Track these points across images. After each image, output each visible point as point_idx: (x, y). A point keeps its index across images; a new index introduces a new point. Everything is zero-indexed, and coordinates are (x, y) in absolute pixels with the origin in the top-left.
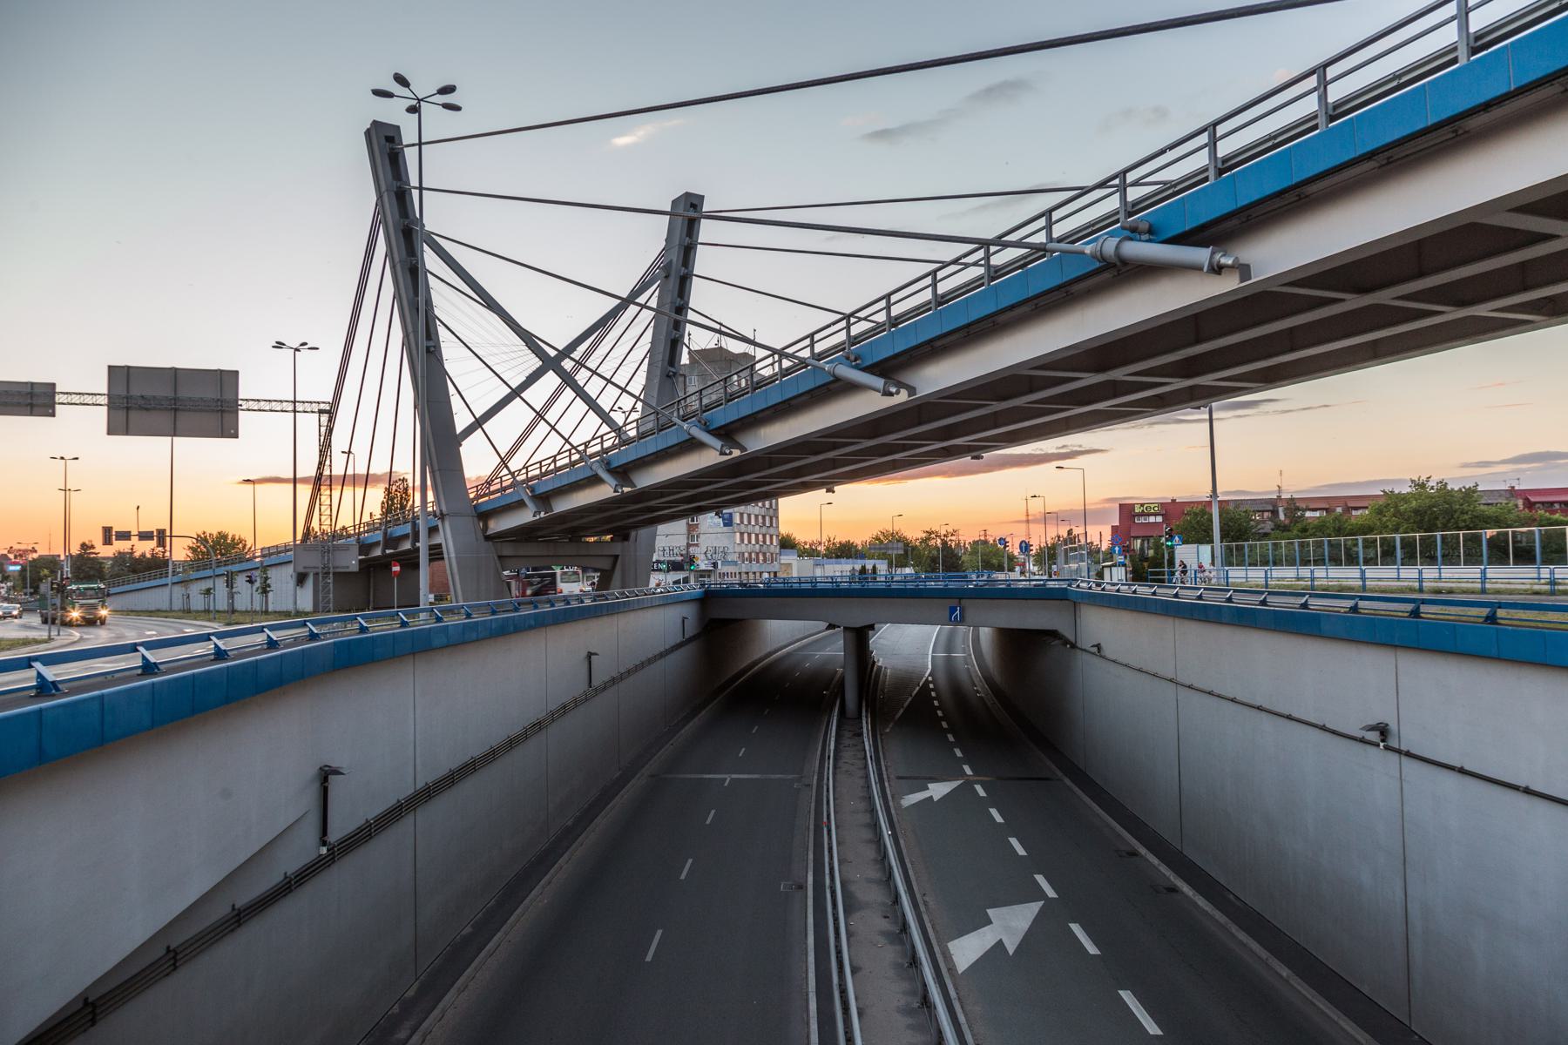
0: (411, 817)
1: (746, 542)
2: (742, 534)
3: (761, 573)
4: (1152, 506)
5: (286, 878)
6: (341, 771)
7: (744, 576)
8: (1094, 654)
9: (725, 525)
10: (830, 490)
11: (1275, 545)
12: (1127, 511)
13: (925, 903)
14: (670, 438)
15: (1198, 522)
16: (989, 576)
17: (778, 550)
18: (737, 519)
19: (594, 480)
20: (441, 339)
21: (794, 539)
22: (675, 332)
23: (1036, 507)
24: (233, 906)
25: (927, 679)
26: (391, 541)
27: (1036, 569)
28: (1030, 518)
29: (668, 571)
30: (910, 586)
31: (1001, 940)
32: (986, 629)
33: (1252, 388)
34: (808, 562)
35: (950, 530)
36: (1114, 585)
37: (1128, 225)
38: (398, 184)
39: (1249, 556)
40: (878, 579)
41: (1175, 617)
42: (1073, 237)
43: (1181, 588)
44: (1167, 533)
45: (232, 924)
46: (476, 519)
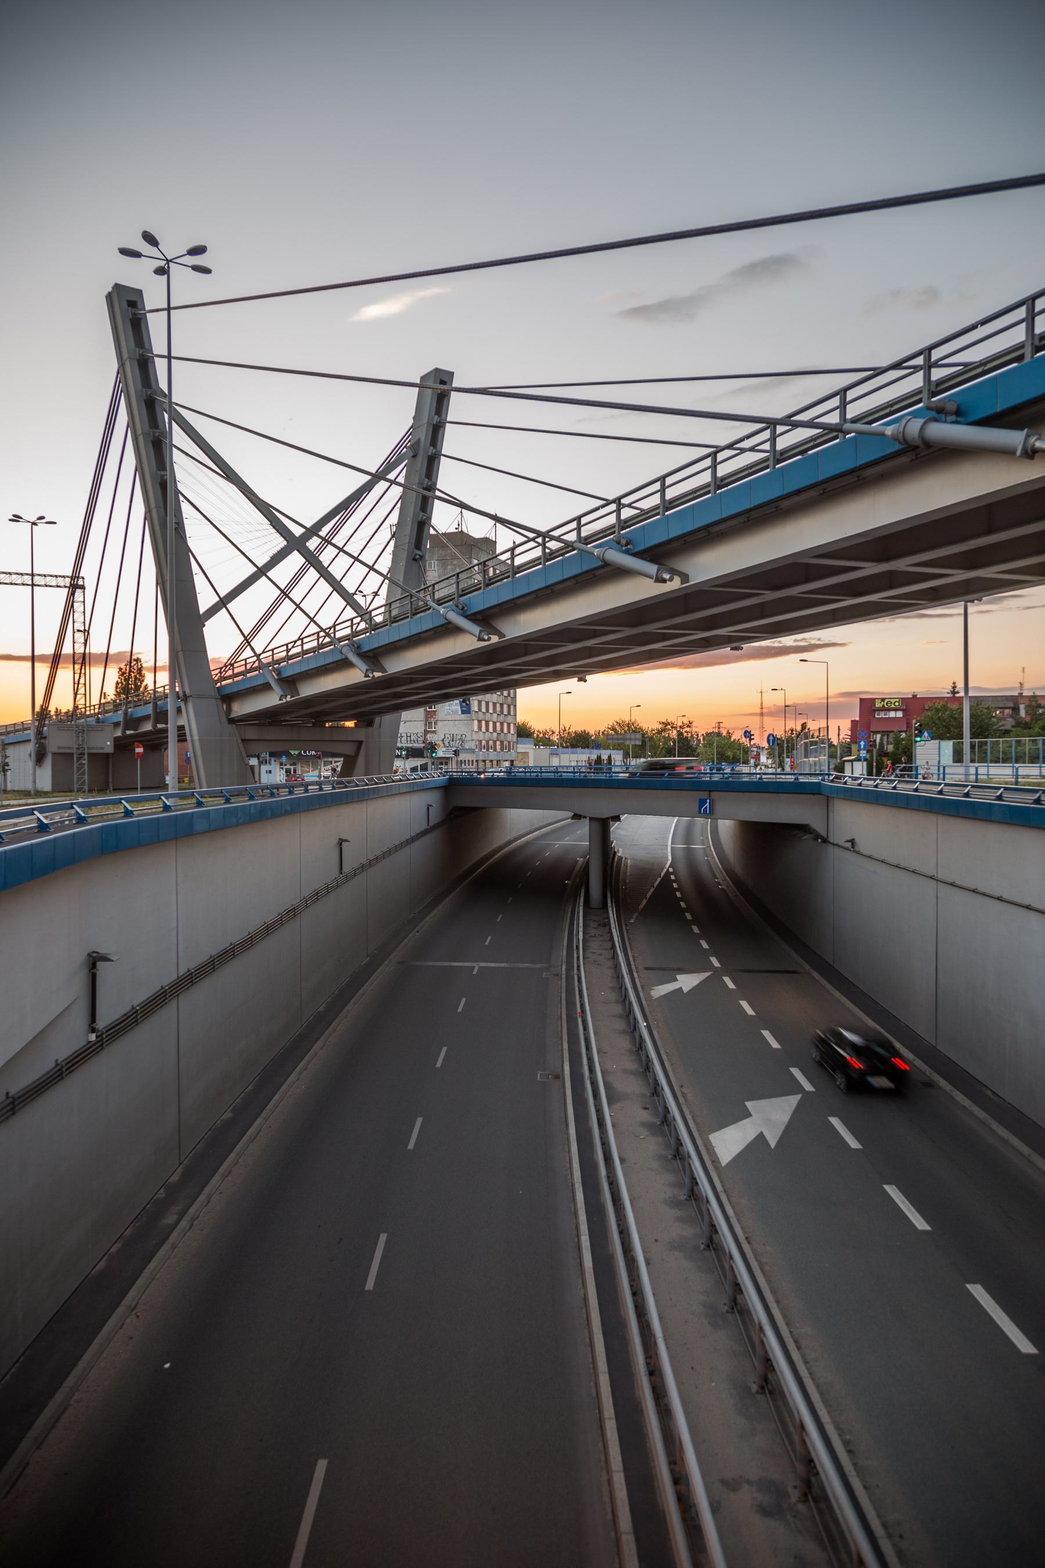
0: (174, 1003)
1: (484, 729)
2: (480, 722)
4: (893, 701)
5: (57, 1065)
6: (109, 957)
7: (481, 764)
8: (847, 849)
9: (463, 712)
10: (582, 679)
11: (1018, 742)
12: (868, 705)
13: (684, 1095)
14: (424, 623)
15: (939, 718)
16: (733, 769)
17: (515, 739)
19: (343, 664)
20: (184, 516)
21: (530, 728)
22: (422, 513)
23: (774, 700)
24: (7, 1093)
25: (668, 870)
26: (131, 722)
27: (770, 761)
29: (407, 758)
33: (1032, 582)
34: (544, 751)
36: (855, 779)
37: (934, 405)
38: (141, 352)
39: (991, 753)
40: (613, 770)
41: (937, 813)
43: (921, 783)
44: (916, 730)
45: (7, 1112)
46: (219, 701)
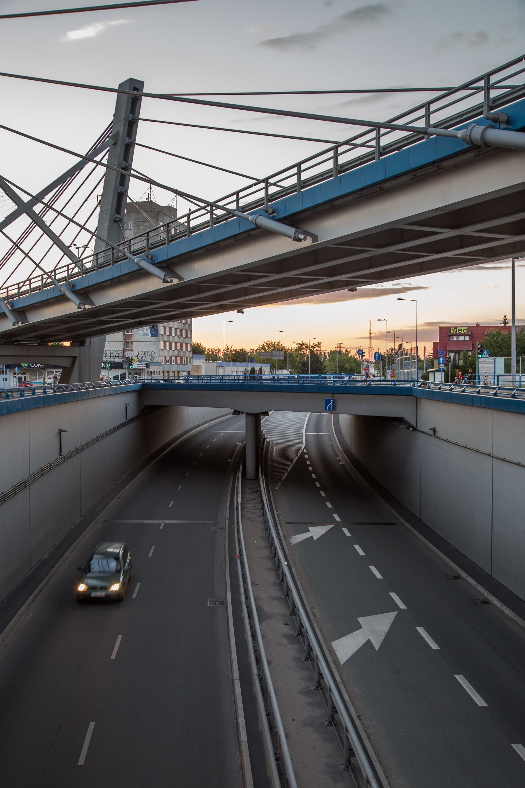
1: (168, 348)
2: (165, 342)
3: (179, 372)
4: (463, 329)
7: (166, 374)
9: (152, 335)
13: (314, 614)
14: (123, 268)
15: (495, 341)
18: (161, 331)
19: (62, 299)
21: (202, 347)
22: (121, 187)
27: (376, 372)
28: (372, 335)
29: (111, 369)
30: (285, 383)
31: (369, 640)
32: (346, 416)
34: (213, 364)
35: (316, 343)
36: (436, 385)
37: (491, 116)
40: (263, 378)
42: (446, 124)
44: (479, 349)
